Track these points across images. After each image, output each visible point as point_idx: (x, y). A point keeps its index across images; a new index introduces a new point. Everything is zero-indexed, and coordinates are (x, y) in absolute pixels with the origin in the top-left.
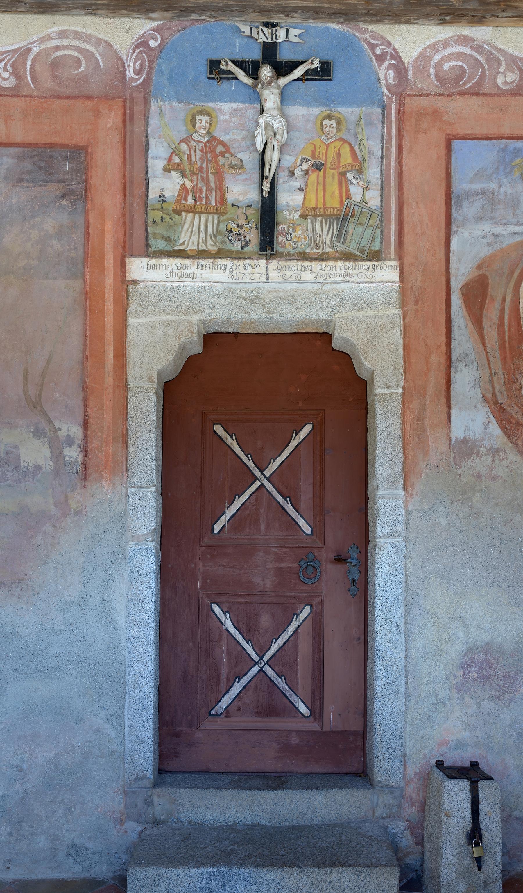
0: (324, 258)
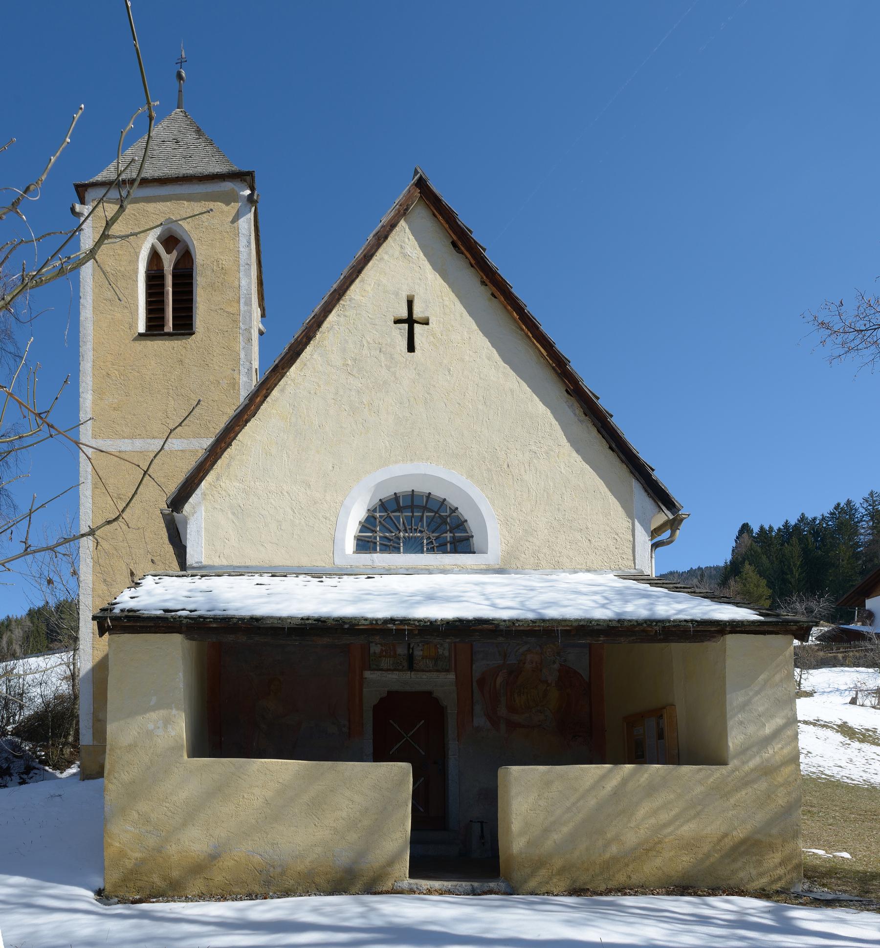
0: (430, 671)
